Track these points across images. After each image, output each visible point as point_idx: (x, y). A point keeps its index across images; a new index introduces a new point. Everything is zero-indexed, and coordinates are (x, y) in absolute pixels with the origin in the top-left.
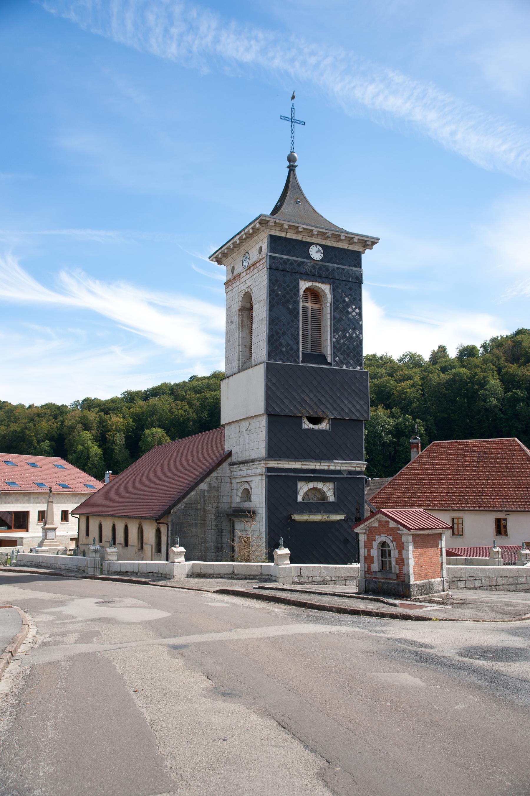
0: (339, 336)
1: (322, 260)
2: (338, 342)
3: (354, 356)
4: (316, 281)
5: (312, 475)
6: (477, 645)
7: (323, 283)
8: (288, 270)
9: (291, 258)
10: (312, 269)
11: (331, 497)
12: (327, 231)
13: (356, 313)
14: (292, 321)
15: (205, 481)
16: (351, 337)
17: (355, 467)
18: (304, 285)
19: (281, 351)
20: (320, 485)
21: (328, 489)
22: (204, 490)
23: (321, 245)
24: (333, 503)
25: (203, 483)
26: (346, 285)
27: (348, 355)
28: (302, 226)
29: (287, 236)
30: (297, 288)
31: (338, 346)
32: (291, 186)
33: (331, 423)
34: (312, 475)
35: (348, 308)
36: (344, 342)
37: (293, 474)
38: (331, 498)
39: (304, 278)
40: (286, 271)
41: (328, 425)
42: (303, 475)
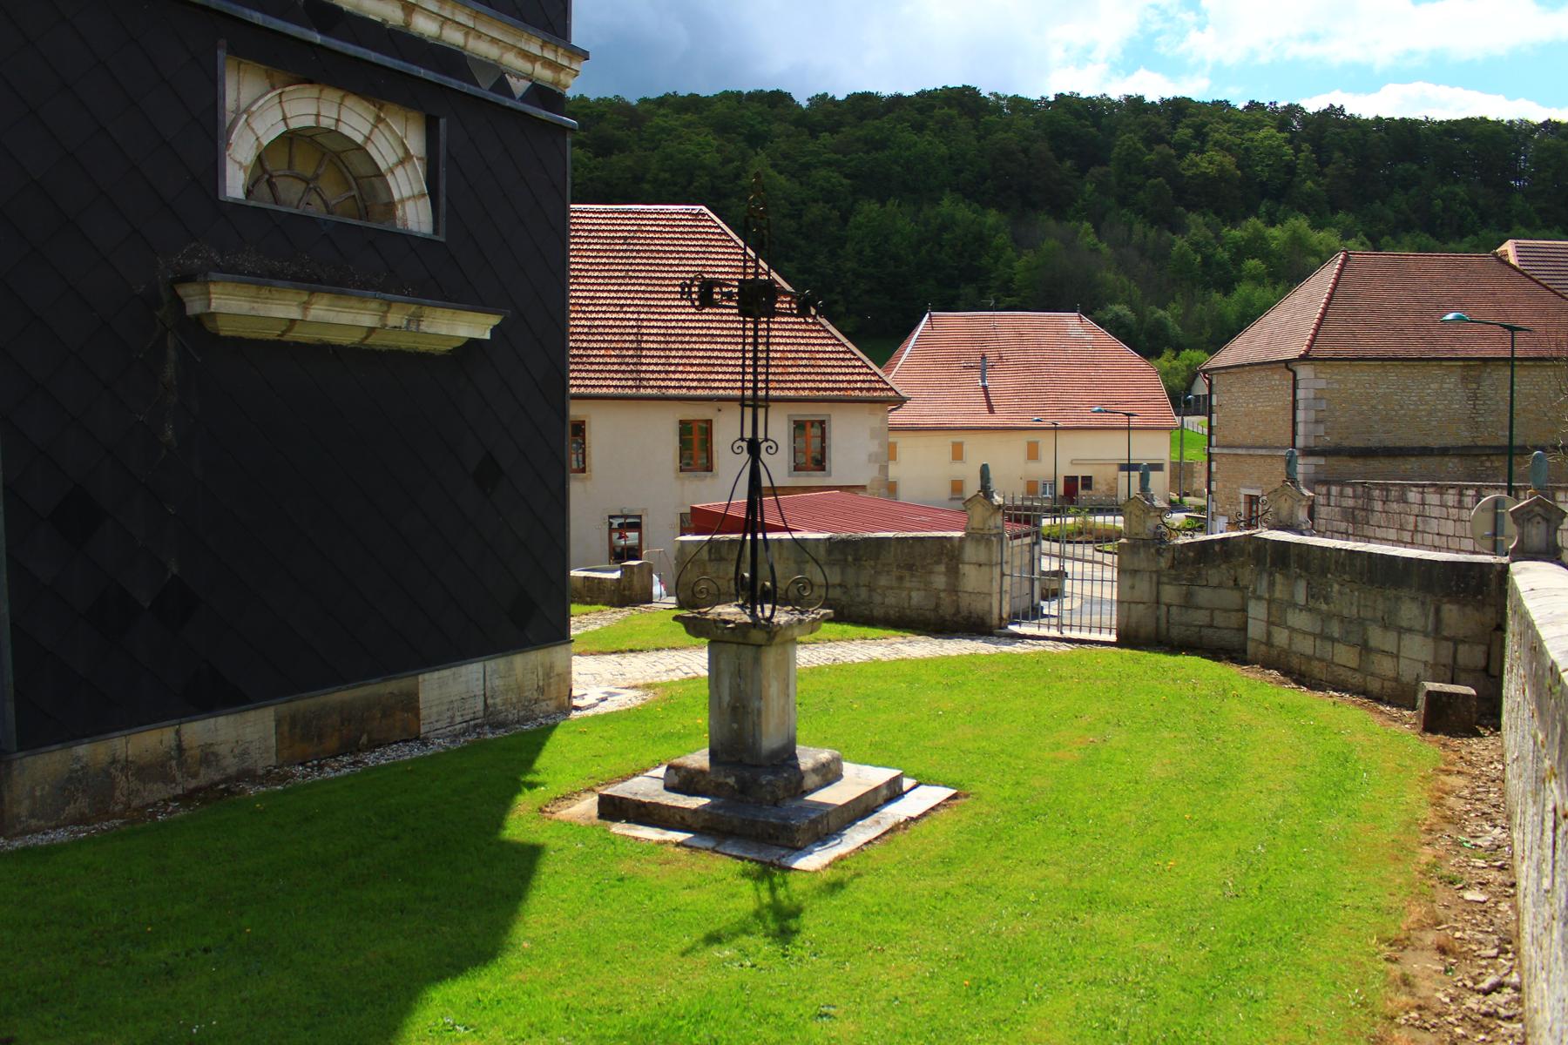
5: (318, 38)
6: (523, 907)
11: (410, 205)
34: (318, 38)
38: (416, 217)
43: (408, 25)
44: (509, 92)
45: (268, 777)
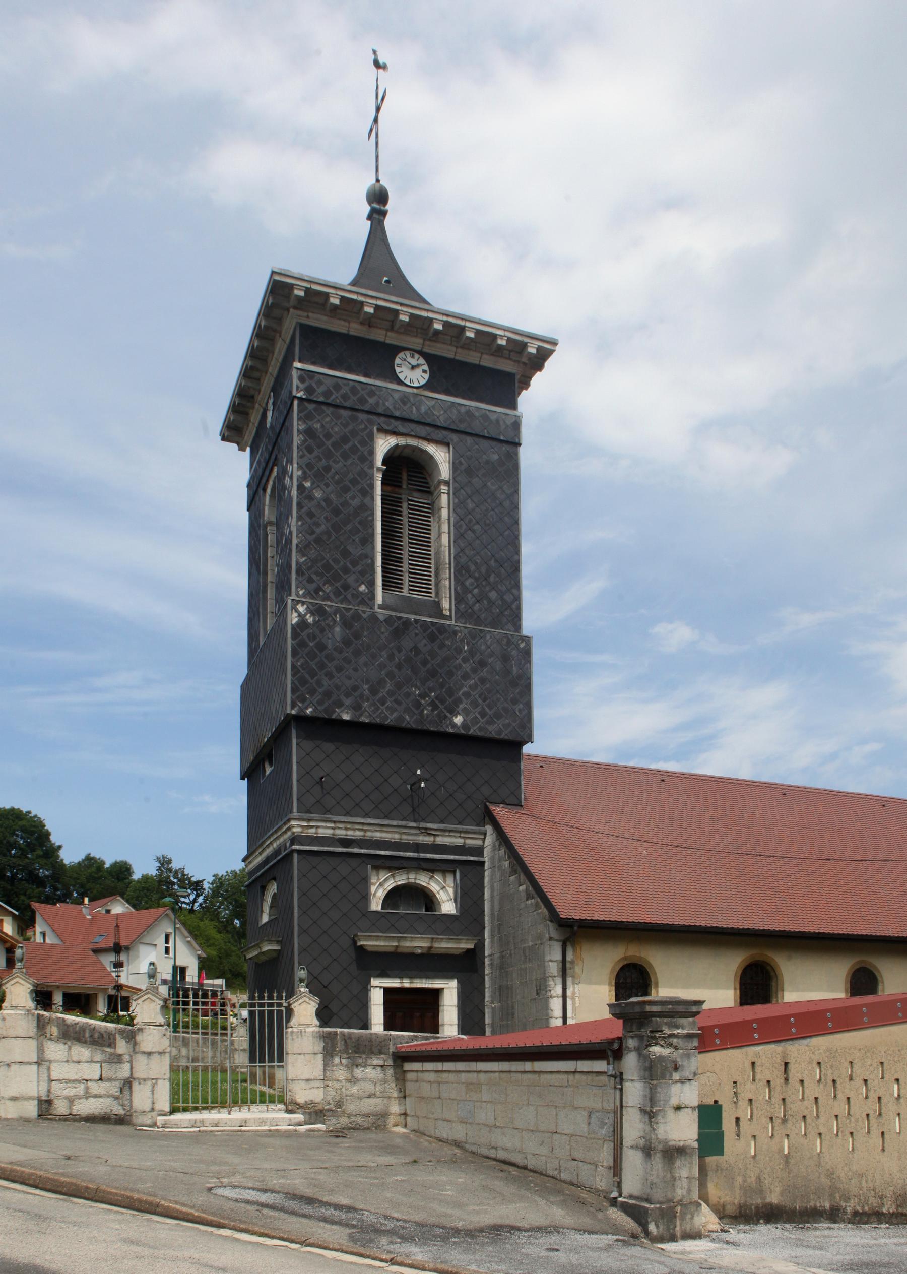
18: (383, 445)
38: (448, 907)
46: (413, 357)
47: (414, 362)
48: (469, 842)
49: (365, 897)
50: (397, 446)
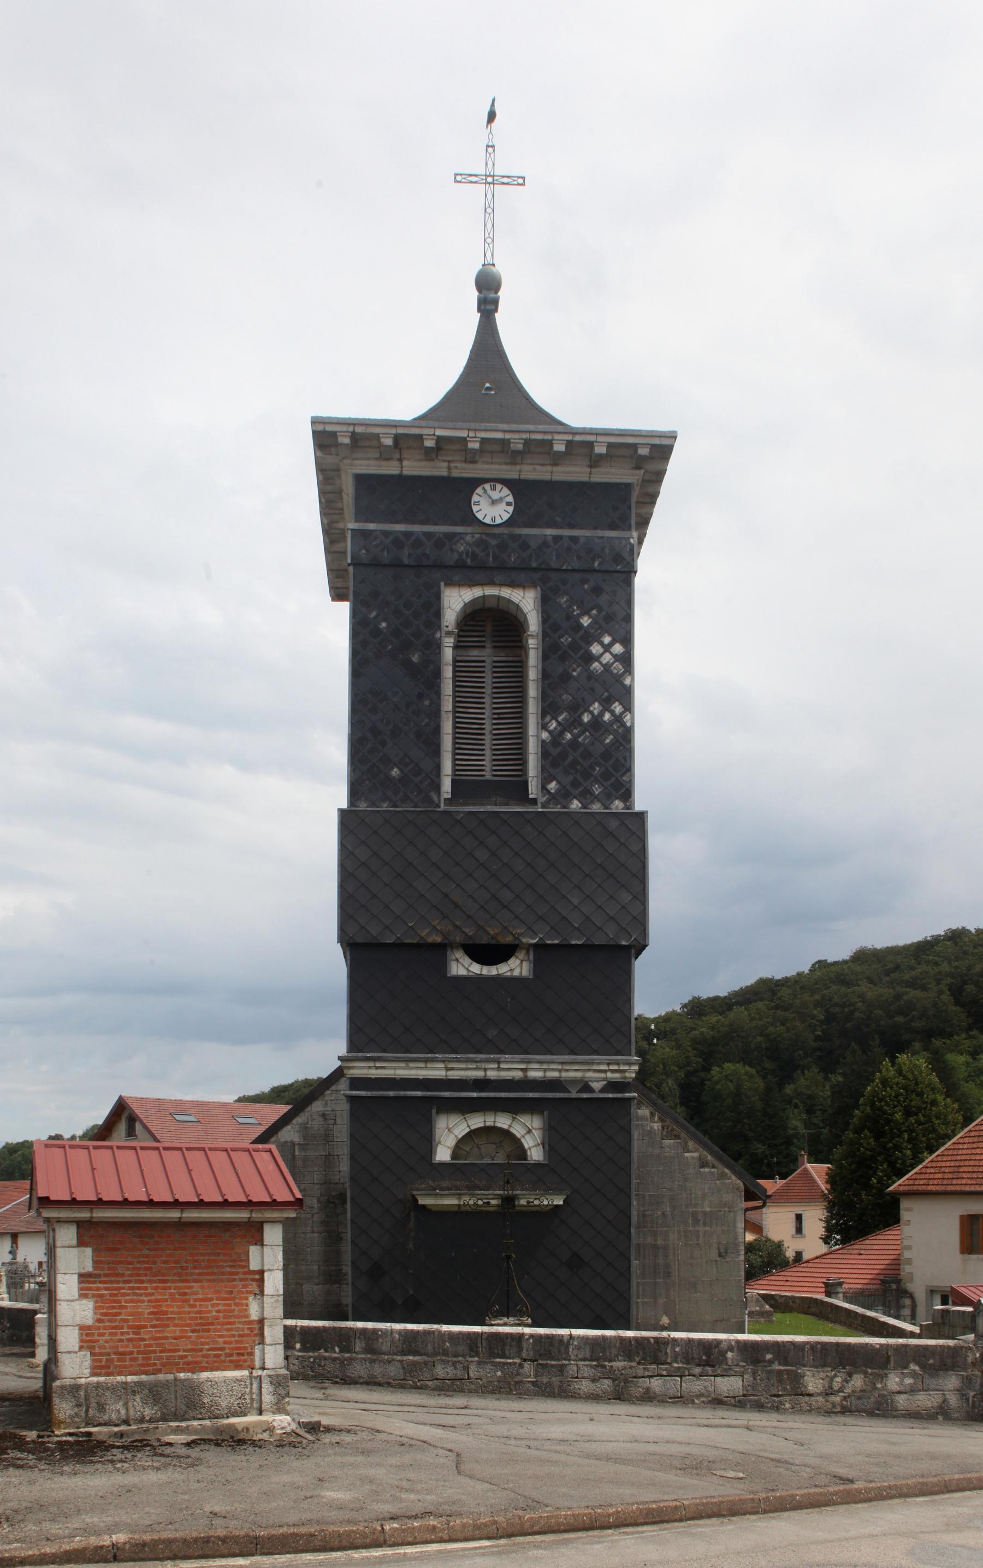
0: (559, 723)
1: (508, 523)
2: (556, 738)
3: (606, 776)
4: (492, 583)
5: (475, 1095)
7: (513, 585)
8: (406, 562)
9: (416, 528)
10: (477, 550)
12: (507, 436)
13: (615, 656)
14: (420, 696)
15: (294, 1121)
16: (596, 723)
17: (605, 1071)
18: (455, 601)
19: (389, 778)
20: (503, 1121)
21: (529, 1133)
22: (293, 1144)
23: (507, 483)
24: (538, 1165)
25: (289, 1127)
26: (584, 581)
27: (587, 774)
28: (431, 431)
29: (406, 472)
30: (435, 609)
31: (555, 752)
32: (488, 354)
33: (531, 957)
35: (590, 644)
36: (575, 738)
37: (419, 1093)
38: (536, 1154)
39: (457, 578)
40: (403, 566)
41: (526, 966)
42: (447, 1094)
43: (526, 1077)
44: (591, 1090)
45: (251, 1292)
46: (494, 489)
47: (495, 495)
48: (564, 1074)
49: (429, 1142)
50: (474, 601)
